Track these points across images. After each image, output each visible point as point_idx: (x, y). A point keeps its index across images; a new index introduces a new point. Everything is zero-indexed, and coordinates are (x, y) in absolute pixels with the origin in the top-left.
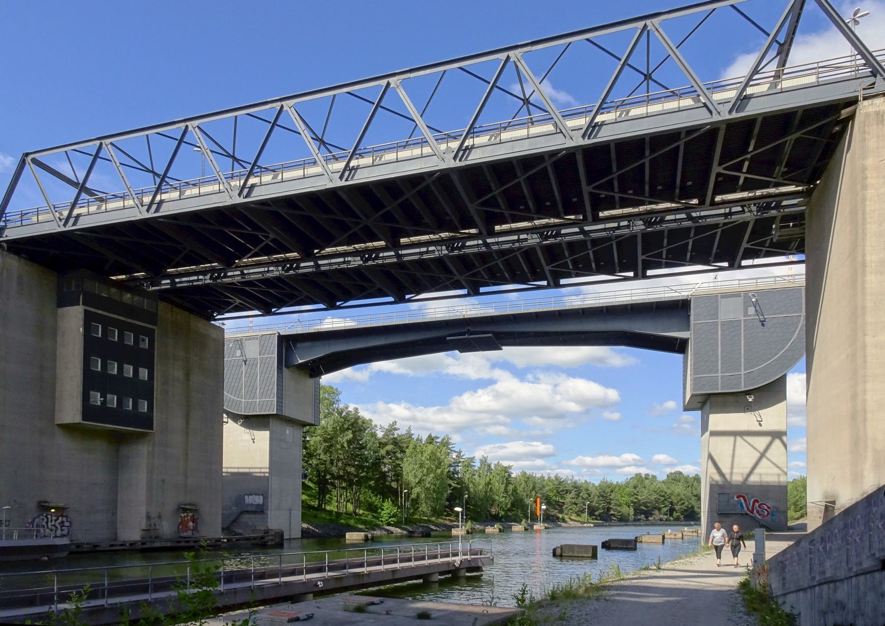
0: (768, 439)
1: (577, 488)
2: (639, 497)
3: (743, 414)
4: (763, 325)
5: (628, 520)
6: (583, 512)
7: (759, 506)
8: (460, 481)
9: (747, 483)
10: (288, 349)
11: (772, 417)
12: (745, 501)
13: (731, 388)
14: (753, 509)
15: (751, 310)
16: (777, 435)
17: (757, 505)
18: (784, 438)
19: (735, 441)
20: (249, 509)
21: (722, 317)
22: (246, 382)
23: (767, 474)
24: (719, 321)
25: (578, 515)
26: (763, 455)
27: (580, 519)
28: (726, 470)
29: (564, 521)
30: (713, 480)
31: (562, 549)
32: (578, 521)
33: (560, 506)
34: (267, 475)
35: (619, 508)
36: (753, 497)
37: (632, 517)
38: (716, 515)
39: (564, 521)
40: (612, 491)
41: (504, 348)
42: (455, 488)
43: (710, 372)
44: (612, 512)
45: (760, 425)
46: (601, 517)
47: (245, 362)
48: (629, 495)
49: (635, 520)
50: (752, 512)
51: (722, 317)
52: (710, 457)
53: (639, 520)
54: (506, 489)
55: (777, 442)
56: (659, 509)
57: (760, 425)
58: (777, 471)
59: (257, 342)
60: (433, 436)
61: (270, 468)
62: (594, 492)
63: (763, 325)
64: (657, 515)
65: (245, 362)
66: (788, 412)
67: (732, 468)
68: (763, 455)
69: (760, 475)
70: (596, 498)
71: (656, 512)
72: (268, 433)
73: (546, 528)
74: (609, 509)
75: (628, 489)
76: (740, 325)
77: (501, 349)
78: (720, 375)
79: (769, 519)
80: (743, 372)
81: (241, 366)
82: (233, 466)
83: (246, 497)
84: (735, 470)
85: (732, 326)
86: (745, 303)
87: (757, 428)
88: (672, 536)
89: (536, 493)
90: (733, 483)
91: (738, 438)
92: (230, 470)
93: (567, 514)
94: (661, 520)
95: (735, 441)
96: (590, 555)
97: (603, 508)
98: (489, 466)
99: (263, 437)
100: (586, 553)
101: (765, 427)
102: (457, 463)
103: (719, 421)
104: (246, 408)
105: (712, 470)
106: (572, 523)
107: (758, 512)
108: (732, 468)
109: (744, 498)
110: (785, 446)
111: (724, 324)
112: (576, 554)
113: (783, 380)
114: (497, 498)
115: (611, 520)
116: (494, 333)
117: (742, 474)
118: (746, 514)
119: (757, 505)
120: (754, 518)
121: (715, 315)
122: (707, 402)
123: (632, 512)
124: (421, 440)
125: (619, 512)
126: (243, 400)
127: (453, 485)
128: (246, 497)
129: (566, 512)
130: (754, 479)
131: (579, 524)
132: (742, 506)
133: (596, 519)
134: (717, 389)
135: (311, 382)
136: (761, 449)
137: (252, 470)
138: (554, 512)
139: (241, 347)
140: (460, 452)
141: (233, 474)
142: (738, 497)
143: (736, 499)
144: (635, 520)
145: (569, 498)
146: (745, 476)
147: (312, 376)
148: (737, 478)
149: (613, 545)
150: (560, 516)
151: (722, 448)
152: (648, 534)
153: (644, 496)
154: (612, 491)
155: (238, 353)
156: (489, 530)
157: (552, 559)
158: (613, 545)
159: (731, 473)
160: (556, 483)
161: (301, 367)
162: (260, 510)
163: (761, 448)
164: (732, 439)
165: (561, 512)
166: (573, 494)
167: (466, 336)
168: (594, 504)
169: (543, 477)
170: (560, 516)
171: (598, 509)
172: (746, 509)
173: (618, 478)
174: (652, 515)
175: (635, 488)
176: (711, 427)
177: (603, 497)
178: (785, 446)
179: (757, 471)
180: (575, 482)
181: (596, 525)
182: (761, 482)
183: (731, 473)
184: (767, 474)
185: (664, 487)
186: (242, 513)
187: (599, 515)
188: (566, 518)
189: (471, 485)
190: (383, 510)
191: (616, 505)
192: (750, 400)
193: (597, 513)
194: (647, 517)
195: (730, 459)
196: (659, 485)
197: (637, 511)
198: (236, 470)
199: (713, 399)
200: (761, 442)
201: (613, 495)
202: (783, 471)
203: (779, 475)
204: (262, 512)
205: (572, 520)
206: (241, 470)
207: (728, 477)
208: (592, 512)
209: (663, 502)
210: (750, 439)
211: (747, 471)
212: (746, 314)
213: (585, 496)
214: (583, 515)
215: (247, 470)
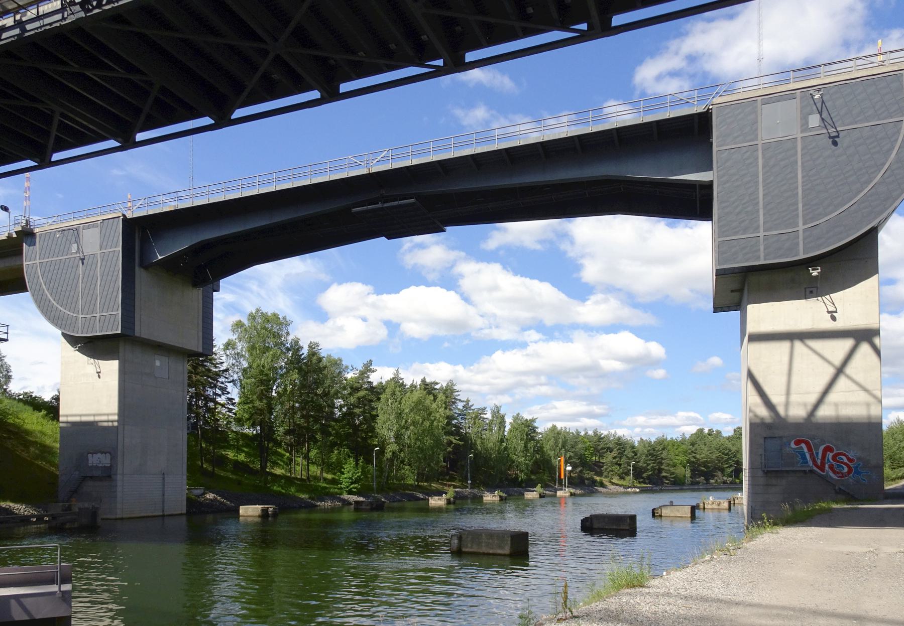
0: (849, 343)
1: (621, 445)
2: (698, 456)
3: (803, 301)
4: (835, 143)
5: (683, 484)
6: (627, 474)
7: (834, 458)
8: (464, 438)
9: (813, 420)
10: (144, 241)
11: (853, 304)
12: (810, 449)
13: (780, 256)
14: (823, 464)
15: (814, 120)
16: (865, 336)
17: (830, 455)
18: (877, 341)
19: (792, 348)
20: (97, 473)
21: (765, 135)
22: (84, 289)
23: (847, 403)
24: (760, 142)
25: (622, 478)
26: (840, 371)
27: (624, 483)
28: (777, 399)
29: (602, 485)
30: (756, 416)
31: (460, 538)
32: (620, 486)
33: (597, 468)
34: (116, 424)
35: (672, 469)
36: (823, 442)
37: (688, 480)
38: (760, 473)
39: (602, 485)
40: (663, 449)
41: (448, 228)
42: (457, 446)
43: (745, 231)
44: (664, 474)
45: (834, 319)
46: (649, 479)
47: (83, 260)
48: (685, 453)
49: (693, 484)
50: (822, 468)
51: (765, 135)
52: (751, 376)
53: (698, 483)
54: (525, 446)
55: (865, 348)
56: (722, 470)
57: (834, 319)
58: (863, 396)
59: (98, 230)
60: (428, 380)
61: (119, 414)
62: (642, 450)
63: (835, 143)
64: (720, 477)
65: (83, 260)
66: (881, 284)
67: (788, 393)
68: (840, 371)
69: (836, 405)
70: (644, 457)
71: (719, 474)
72: (115, 363)
73: (572, 495)
74: (660, 470)
75: (683, 446)
76: (795, 147)
77: (444, 231)
78: (762, 234)
79: (850, 479)
80: (801, 227)
81: (78, 266)
82: (74, 412)
83: (90, 456)
84: (794, 398)
85: (781, 150)
86: (802, 108)
87: (826, 324)
88: (715, 506)
89: (566, 451)
90: (790, 420)
91: (798, 344)
92: (71, 419)
93: (606, 477)
94: (725, 482)
95: (792, 348)
96: (507, 550)
97: (653, 469)
98: (503, 418)
99: (111, 368)
100: (500, 547)
101: (842, 323)
102: (463, 415)
103: (765, 315)
104: (83, 327)
105: (754, 399)
106: (612, 487)
107: (831, 467)
108: (788, 393)
109: (807, 443)
110: (877, 351)
111: (767, 147)
112: (484, 550)
113: (869, 239)
114: (514, 457)
115: (663, 483)
116: (418, 196)
117: (805, 405)
118: (811, 471)
119: (830, 455)
120: (825, 480)
121: (754, 133)
122: (739, 285)
123: (688, 473)
124: (416, 387)
125: (673, 473)
126: (80, 316)
127: (454, 441)
128: (90, 456)
129: (605, 474)
130: (825, 412)
131: (622, 489)
132: (804, 458)
133: (645, 483)
134: (758, 258)
135: (197, 294)
136: (838, 361)
137: (97, 418)
138: (588, 474)
139: (78, 240)
140: (468, 401)
141: (74, 424)
142: (797, 443)
143: (793, 445)
144: (693, 484)
145: (609, 458)
146: (810, 408)
147: (195, 285)
148: (797, 412)
149: (596, 525)
150: (598, 478)
151: (769, 361)
152: (671, 504)
153: (703, 454)
154: (663, 449)
155: (74, 247)
156: (529, 495)
157: (652, 520)
158: (596, 525)
159: (787, 405)
160: (596, 439)
161: (172, 266)
162: (108, 474)
163: (838, 360)
164: (785, 345)
165: (600, 474)
166: (615, 453)
167: (379, 205)
168: (640, 464)
169: (578, 433)
170: (598, 478)
171: (646, 470)
172: (811, 463)
173: (673, 435)
174: (713, 477)
175: (693, 444)
176: (751, 328)
177: (653, 455)
178: (877, 351)
179: (832, 397)
180: (619, 438)
181: (643, 491)
182: (837, 417)
183: (787, 405)
184: (846, 404)
185: (729, 445)
186: (85, 478)
187: (649, 477)
188: (606, 481)
189: (479, 442)
190: (343, 473)
191: (668, 465)
192: (815, 273)
193: (644, 475)
194: (707, 480)
195: (784, 379)
196: (722, 441)
197: (695, 472)
198: (77, 419)
199: (753, 278)
200: (838, 349)
201: (665, 453)
202: (874, 396)
203: (868, 405)
204: (110, 477)
205: (613, 484)
206: (84, 419)
207: (781, 410)
208: (638, 474)
209: (727, 461)
210: (816, 344)
211: (813, 398)
212: (805, 127)
213: (631, 455)
214: (627, 478)
215: (91, 419)
